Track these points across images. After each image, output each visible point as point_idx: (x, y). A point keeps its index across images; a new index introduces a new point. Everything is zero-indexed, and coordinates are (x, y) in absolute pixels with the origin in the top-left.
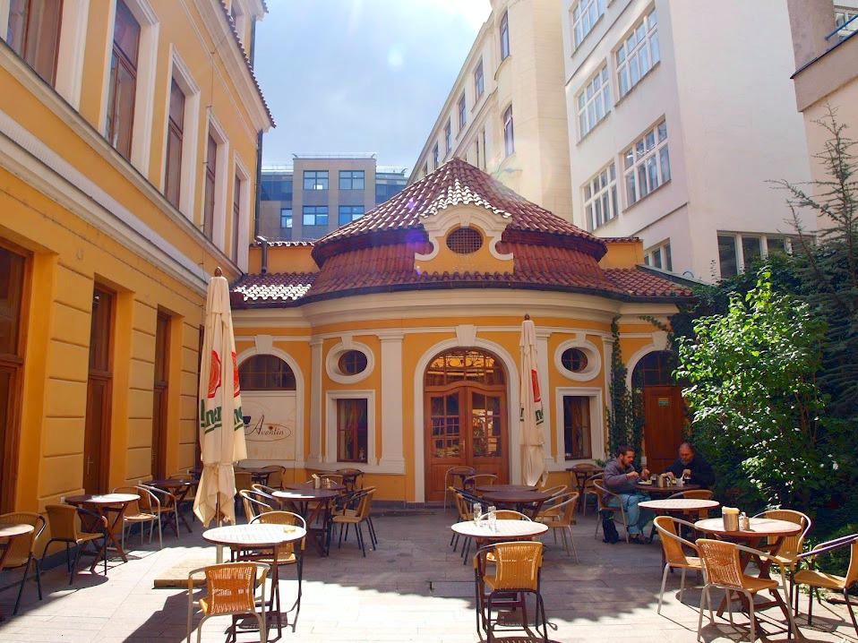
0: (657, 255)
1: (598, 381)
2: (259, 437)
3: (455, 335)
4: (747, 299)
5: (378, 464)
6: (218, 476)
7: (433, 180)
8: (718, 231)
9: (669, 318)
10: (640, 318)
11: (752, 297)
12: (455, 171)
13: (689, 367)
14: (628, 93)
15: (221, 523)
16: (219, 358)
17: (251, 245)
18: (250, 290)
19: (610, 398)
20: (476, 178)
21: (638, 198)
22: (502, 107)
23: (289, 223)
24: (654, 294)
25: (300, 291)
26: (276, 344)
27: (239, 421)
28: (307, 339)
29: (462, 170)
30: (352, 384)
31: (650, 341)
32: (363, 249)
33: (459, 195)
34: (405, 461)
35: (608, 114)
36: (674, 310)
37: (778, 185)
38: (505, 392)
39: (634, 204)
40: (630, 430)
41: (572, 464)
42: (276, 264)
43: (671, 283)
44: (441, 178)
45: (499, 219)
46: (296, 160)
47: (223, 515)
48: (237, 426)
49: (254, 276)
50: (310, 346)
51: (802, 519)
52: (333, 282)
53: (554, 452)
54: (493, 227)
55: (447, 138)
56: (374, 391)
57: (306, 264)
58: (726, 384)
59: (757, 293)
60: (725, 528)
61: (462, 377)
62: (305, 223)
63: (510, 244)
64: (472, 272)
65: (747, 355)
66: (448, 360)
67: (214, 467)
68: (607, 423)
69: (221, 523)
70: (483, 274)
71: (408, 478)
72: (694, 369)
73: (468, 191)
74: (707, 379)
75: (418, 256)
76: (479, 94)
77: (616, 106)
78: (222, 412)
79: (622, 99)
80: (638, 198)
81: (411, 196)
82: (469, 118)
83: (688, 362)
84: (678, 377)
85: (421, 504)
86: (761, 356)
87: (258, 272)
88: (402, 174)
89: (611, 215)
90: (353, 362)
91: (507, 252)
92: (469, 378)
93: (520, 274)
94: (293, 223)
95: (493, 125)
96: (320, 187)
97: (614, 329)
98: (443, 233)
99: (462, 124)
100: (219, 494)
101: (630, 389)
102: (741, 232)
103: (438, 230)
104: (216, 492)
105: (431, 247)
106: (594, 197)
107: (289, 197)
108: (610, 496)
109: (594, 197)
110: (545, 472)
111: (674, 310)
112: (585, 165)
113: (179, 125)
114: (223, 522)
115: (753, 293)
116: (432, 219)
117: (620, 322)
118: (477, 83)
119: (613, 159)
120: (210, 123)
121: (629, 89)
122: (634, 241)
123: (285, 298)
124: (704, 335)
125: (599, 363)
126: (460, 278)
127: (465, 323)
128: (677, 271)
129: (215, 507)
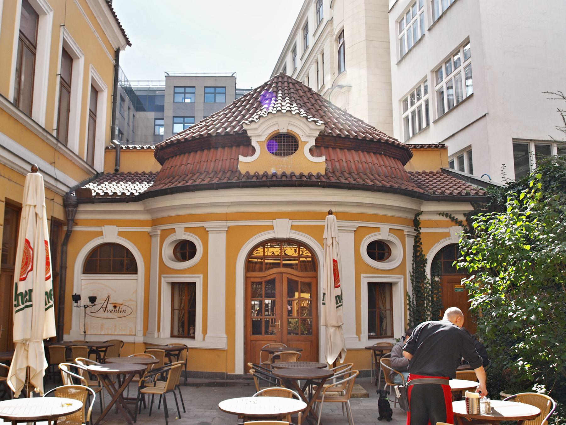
0: (461, 159)
1: (401, 269)
2: (105, 315)
3: (272, 227)
4: (521, 198)
5: (204, 340)
6: (28, 351)
7: (260, 92)
8: (513, 139)
9: (465, 215)
10: (439, 214)
11: (526, 196)
12: (280, 84)
13: (468, 259)
14: (440, 18)
15: (31, 393)
16: (32, 245)
17: (107, 148)
18: (100, 187)
19: (411, 285)
20: (297, 90)
21: (446, 110)
22: (336, 32)
23: (162, 131)
24: (451, 194)
25: (141, 188)
26: (120, 234)
27: (49, 302)
28: (148, 229)
29: (286, 84)
30: (184, 271)
31: (447, 235)
32: (202, 150)
33: (279, 105)
34: (227, 338)
35: (423, 36)
37: (554, 96)
38: (316, 278)
39: (443, 115)
40: (429, 313)
41: (373, 343)
42: (129, 164)
43: (469, 184)
44: (268, 90)
45: (313, 126)
46: (168, 77)
47: (32, 387)
48: (47, 306)
49: (109, 174)
50: (150, 236)
51: (549, 402)
52: (168, 181)
53: (358, 332)
54: (307, 132)
55: (294, 59)
56: (202, 276)
57: (151, 164)
58: (502, 275)
59: (529, 192)
60: (468, 412)
61: (277, 265)
62: (174, 132)
63: (323, 148)
64: (306, 174)
65: (519, 249)
66: (283, 249)
67: (25, 343)
68: (408, 307)
69: (31, 393)
70: (297, 174)
71: (226, 354)
72: (472, 261)
73: (288, 101)
74: (483, 269)
75: (241, 158)
76: (319, 21)
77: (429, 30)
78: (34, 295)
79: (435, 24)
80: (446, 110)
81: (241, 106)
82: (311, 41)
83: (467, 254)
84: (458, 268)
85: (241, 375)
86: (532, 249)
87: (112, 171)
89: (424, 125)
90: (185, 250)
91: (320, 155)
92: (285, 266)
93: (330, 175)
94: (165, 132)
95: (329, 48)
96: (188, 101)
97: (416, 224)
98: (263, 138)
99: (306, 47)
100: (28, 368)
101: (429, 277)
102: (534, 140)
103: (260, 131)
104: (25, 366)
105: (254, 150)
106: (410, 110)
107: (161, 109)
108: (395, 374)
109: (410, 110)
110: (343, 350)
112: (404, 79)
113: (33, 43)
114: (34, 393)
115: (526, 192)
116: (253, 126)
117: (422, 218)
118: (318, 11)
119: (426, 76)
120: (64, 40)
121: (440, 15)
122: (441, 147)
123: (128, 194)
124: (482, 230)
125: (401, 253)
126: (287, 177)
127: (280, 217)
128: (477, 175)
129: (24, 380)
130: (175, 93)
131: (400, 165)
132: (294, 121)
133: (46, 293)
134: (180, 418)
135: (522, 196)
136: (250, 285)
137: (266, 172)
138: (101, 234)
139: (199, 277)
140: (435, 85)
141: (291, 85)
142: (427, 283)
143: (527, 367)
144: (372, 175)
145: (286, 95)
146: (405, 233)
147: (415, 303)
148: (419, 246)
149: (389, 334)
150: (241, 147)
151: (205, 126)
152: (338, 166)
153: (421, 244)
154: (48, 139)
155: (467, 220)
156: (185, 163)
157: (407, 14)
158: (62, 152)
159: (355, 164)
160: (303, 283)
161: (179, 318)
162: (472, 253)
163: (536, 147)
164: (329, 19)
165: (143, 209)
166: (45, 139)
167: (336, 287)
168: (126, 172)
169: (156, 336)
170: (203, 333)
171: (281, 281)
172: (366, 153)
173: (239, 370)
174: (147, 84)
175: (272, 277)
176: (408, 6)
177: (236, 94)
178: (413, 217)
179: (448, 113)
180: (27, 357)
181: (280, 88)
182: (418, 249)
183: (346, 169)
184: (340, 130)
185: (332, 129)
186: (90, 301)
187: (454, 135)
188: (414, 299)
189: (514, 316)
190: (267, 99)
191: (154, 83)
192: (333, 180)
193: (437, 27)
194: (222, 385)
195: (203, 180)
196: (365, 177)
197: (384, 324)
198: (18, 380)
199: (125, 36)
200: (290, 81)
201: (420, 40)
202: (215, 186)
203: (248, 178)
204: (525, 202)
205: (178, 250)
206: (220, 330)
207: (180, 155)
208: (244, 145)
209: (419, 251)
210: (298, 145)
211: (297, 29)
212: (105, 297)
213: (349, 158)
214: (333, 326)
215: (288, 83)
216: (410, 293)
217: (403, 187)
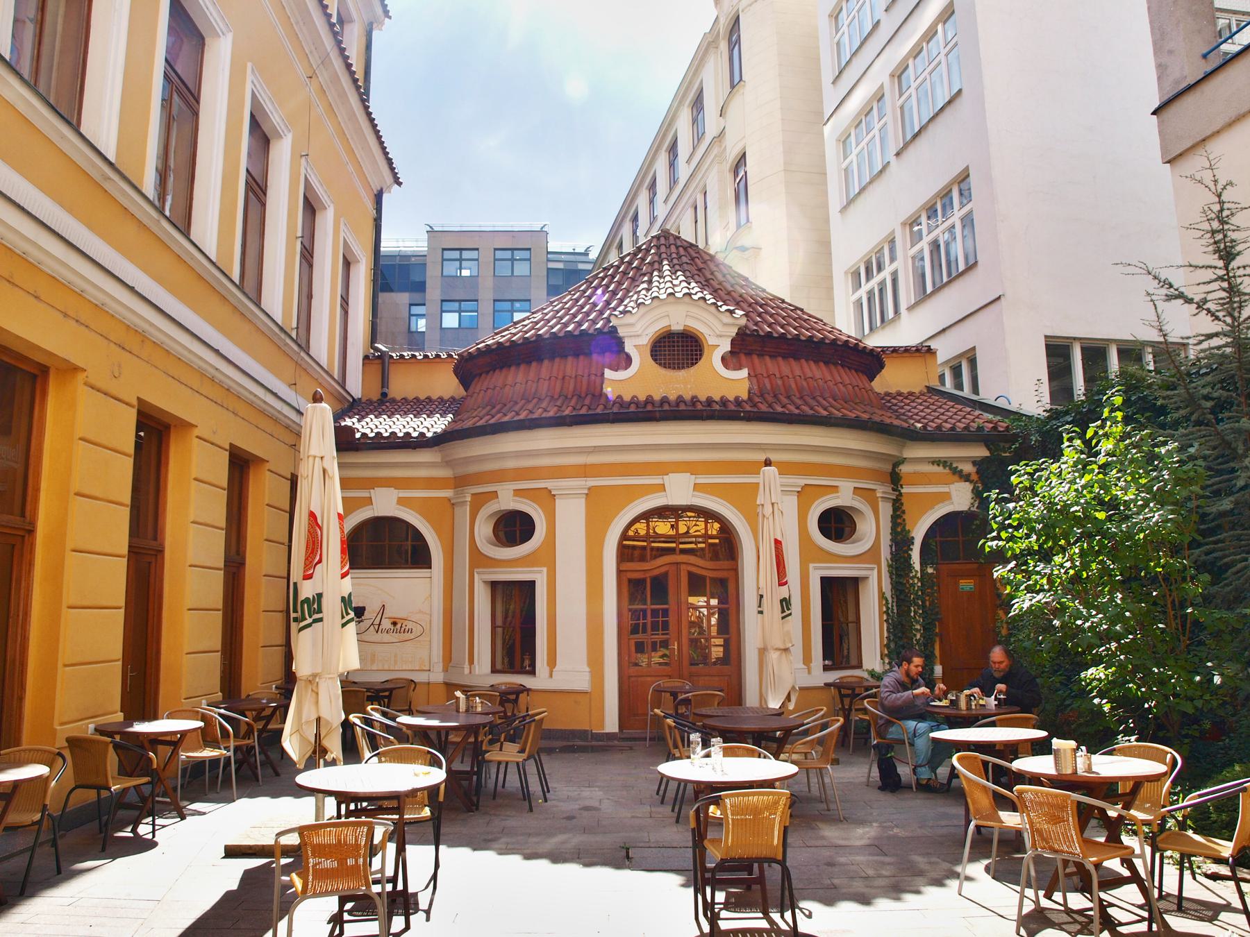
1: (871, 555)
3: (662, 488)
5: (551, 676)
7: (630, 263)
9: (974, 463)
10: (933, 463)
11: (1096, 433)
12: (663, 249)
13: (1004, 535)
14: (916, 136)
15: (322, 761)
17: (366, 358)
18: (363, 423)
21: (929, 289)
23: (421, 325)
24: (953, 429)
25: (435, 424)
26: (402, 502)
27: (348, 614)
28: (447, 493)
29: (673, 249)
30: (512, 563)
31: (946, 497)
33: (669, 285)
36: (981, 452)
38: (735, 571)
39: (923, 297)
41: (833, 676)
42: (403, 385)
43: (977, 412)
44: (643, 259)
45: (727, 319)
46: (432, 232)
47: (324, 751)
49: (370, 402)
52: (484, 411)
53: (807, 659)
54: (718, 331)
55: (651, 202)
56: (545, 570)
57: (446, 384)
59: (1102, 427)
64: (717, 398)
65: (1088, 517)
67: (312, 680)
69: (322, 761)
70: (703, 399)
71: (593, 697)
72: (1011, 538)
73: (682, 278)
74: (1029, 552)
75: (608, 374)
77: (898, 154)
79: (906, 145)
80: (929, 289)
82: (683, 172)
83: (1003, 527)
84: (987, 549)
86: (1109, 519)
87: (375, 396)
88: (586, 254)
90: (514, 528)
92: (684, 551)
93: (757, 399)
95: (718, 182)
96: (466, 273)
97: (895, 479)
98: (646, 340)
99: (673, 181)
100: (318, 720)
101: (917, 566)
102: (1080, 339)
103: (638, 328)
104: (314, 717)
105: (628, 360)
106: (866, 287)
107: (420, 287)
108: (889, 723)
109: (866, 287)
110: (793, 688)
111: (981, 452)
112: (853, 240)
116: (628, 319)
117: (904, 469)
122: (923, 352)
123: (415, 434)
124: (1026, 489)
125: (872, 529)
127: (676, 471)
128: (987, 394)
129: (313, 740)
130: (443, 260)
131: (860, 380)
132: (695, 311)
133: (343, 598)
134: (546, 800)
135: (1090, 433)
136: (625, 583)
138: (369, 501)
139: (540, 572)
140: (909, 246)
141: (681, 251)
142: (915, 577)
143: (1107, 708)
145: (677, 267)
148: (899, 517)
149: (854, 662)
151: (542, 319)
153: (904, 512)
154: (287, 344)
155: (977, 473)
156: (516, 381)
157: (857, 127)
158: (305, 366)
160: (713, 580)
161: (504, 640)
162: (1010, 526)
163: (1120, 352)
164: (715, 133)
165: (439, 460)
166: (281, 345)
167: (781, 584)
168: (399, 398)
169: (467, 671)
170: (548, 664)
171: (678, 576)
172: (812, 363)
173: (611, 724)
174: (395, 244)
175: (663, 570)
176: (859, 114)
177: (548, 260)
178: (889, 468)
179: (933, 293)
180: (317, 702)
181: (664, 256)
183: (782, 390)
184: (770, 325)
185: (756, 324)
187: (944, 330)
189: (1087, 624)
190: (644, 275)
191: (407, 244)
193: (912, 150)
194: (594, 749)
195: (531, 412)
196: (813, 403)
197: (845, 646)
198: (303, 739)
199: (392, 169)
200: (679, 243)
201: (881, 172)
202: (568, 420)
203: (621, 406)
204: (1094, 442)
206: (580, 655)
207: (501, 368)
208: (612, 352)
211: (657, 151)
212: (377, 607)
213: (786, 370)
214: (777, 649)
215: (677, 248)
216: (888, 595)
217: (877, 418)
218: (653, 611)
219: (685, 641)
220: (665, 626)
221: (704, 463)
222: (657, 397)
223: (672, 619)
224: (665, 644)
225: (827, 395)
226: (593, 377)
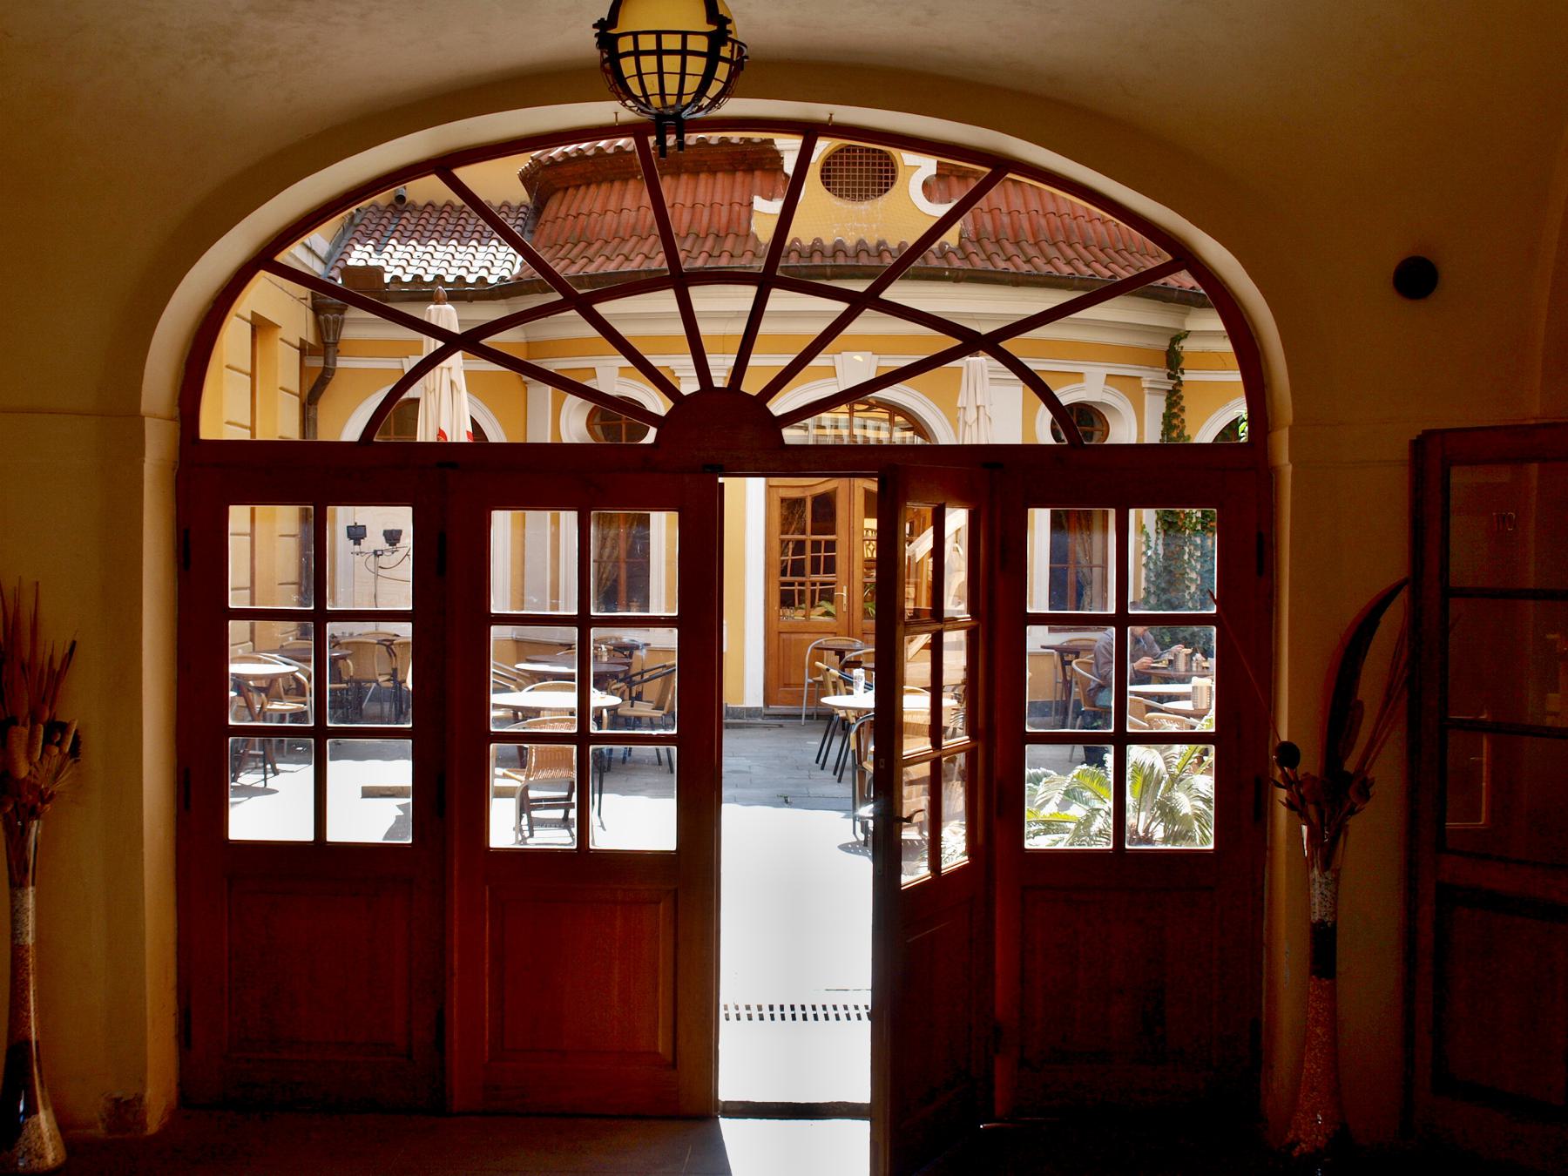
40: (1194, 575)
97: (1173, 361)
136: (777, 504)
137: (818, 240)
144: (1070, 246)
146: (1145, 385)
147: (1161, 551)
148: (1176, 416)
150: (757, 173)
152: (989, 227)
153: (1182, 410)
159: (1030, 220)
178: (1165, 344)
182: (1175, 422)
186: (387, 540)
188: (1160, 542)
192: (980, 263)
205: (597, 420)
208: (763, 169)
209: (1176, 427)
210: (893, 171)
218: (814, 542)
219: (858, 586)
220: (830, 566)
221: (888, 337)
222: (850, 242)
223: (840, 555)
224: (828, 595)
225: (1075, 239)
226: (736, 207)
